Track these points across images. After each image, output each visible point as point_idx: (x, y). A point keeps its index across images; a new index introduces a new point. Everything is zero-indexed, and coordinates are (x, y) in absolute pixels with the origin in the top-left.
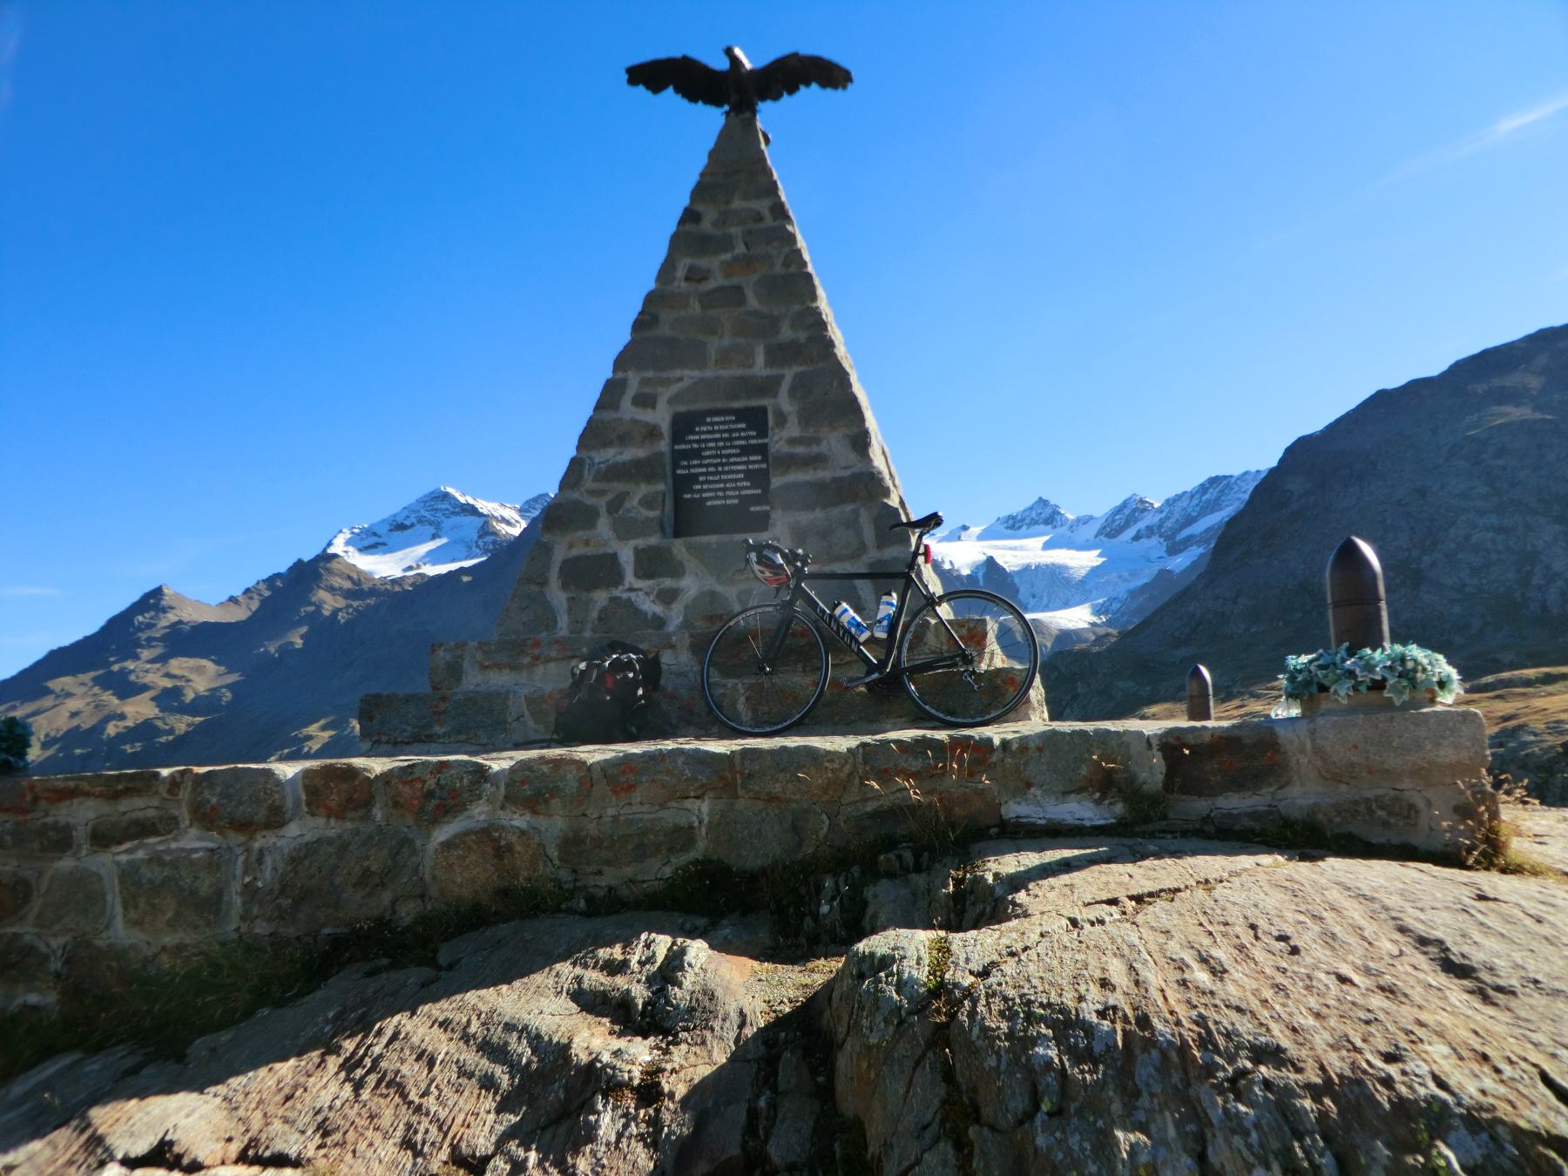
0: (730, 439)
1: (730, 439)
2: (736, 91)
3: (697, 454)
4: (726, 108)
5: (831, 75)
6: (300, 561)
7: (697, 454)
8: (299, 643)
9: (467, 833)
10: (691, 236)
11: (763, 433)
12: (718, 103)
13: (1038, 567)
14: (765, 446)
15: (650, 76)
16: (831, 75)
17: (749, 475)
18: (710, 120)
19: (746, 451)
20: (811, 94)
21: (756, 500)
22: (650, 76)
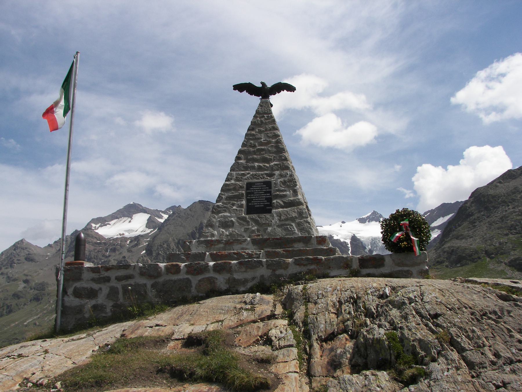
0: (262, 189)
1: (262, 189)
2: (264, 92)
3: (253, 193)
4: (261, 97)
5: (291, 88)
6: (457, 202)
7: (253, 193)
8: (407, 196)
9: (204, 278)
10: (250, 135)
11: (270, 188)
12: (258, 95)
13: (286, 159)
14: (271, 191)
15: (240, 88)
16: (291, 88)
17: (266, 199)
18: (256, 100)
19: (266, 192)
20: (284, 93)
21: (267, 205)
22: (240, 88)
